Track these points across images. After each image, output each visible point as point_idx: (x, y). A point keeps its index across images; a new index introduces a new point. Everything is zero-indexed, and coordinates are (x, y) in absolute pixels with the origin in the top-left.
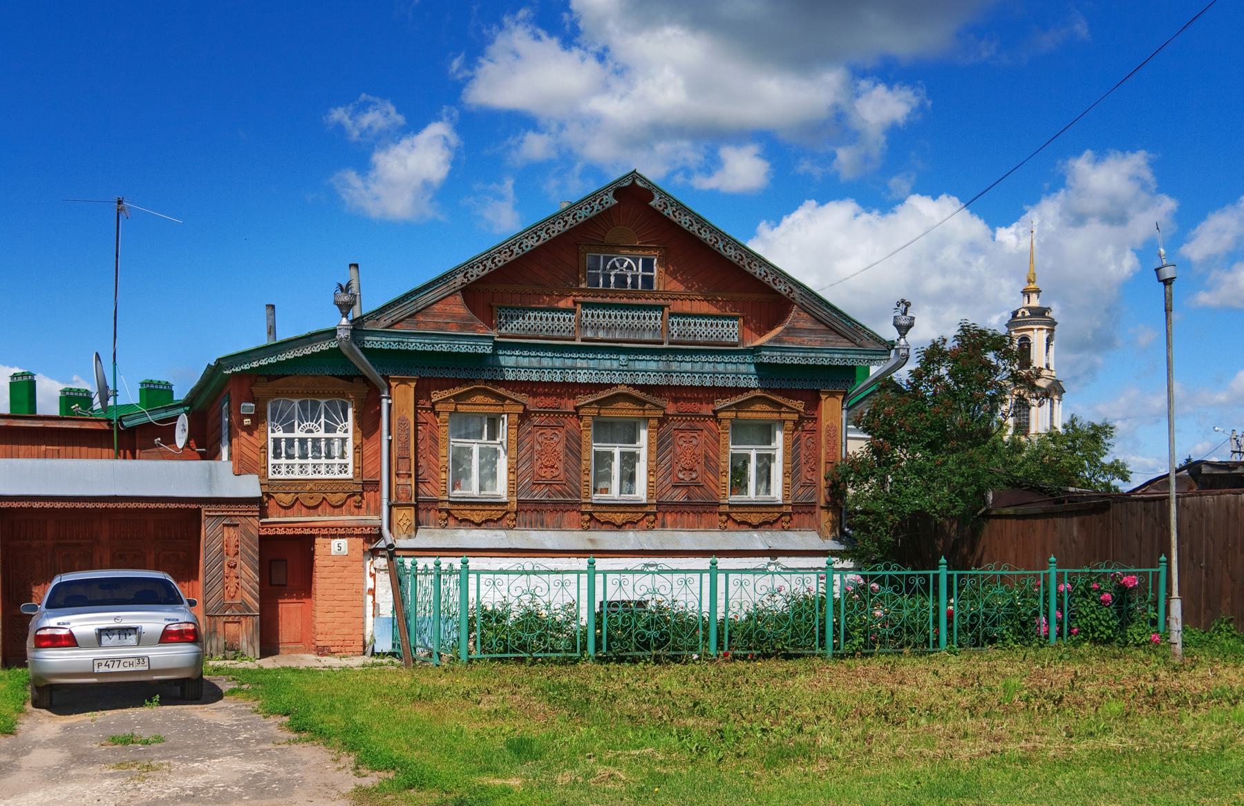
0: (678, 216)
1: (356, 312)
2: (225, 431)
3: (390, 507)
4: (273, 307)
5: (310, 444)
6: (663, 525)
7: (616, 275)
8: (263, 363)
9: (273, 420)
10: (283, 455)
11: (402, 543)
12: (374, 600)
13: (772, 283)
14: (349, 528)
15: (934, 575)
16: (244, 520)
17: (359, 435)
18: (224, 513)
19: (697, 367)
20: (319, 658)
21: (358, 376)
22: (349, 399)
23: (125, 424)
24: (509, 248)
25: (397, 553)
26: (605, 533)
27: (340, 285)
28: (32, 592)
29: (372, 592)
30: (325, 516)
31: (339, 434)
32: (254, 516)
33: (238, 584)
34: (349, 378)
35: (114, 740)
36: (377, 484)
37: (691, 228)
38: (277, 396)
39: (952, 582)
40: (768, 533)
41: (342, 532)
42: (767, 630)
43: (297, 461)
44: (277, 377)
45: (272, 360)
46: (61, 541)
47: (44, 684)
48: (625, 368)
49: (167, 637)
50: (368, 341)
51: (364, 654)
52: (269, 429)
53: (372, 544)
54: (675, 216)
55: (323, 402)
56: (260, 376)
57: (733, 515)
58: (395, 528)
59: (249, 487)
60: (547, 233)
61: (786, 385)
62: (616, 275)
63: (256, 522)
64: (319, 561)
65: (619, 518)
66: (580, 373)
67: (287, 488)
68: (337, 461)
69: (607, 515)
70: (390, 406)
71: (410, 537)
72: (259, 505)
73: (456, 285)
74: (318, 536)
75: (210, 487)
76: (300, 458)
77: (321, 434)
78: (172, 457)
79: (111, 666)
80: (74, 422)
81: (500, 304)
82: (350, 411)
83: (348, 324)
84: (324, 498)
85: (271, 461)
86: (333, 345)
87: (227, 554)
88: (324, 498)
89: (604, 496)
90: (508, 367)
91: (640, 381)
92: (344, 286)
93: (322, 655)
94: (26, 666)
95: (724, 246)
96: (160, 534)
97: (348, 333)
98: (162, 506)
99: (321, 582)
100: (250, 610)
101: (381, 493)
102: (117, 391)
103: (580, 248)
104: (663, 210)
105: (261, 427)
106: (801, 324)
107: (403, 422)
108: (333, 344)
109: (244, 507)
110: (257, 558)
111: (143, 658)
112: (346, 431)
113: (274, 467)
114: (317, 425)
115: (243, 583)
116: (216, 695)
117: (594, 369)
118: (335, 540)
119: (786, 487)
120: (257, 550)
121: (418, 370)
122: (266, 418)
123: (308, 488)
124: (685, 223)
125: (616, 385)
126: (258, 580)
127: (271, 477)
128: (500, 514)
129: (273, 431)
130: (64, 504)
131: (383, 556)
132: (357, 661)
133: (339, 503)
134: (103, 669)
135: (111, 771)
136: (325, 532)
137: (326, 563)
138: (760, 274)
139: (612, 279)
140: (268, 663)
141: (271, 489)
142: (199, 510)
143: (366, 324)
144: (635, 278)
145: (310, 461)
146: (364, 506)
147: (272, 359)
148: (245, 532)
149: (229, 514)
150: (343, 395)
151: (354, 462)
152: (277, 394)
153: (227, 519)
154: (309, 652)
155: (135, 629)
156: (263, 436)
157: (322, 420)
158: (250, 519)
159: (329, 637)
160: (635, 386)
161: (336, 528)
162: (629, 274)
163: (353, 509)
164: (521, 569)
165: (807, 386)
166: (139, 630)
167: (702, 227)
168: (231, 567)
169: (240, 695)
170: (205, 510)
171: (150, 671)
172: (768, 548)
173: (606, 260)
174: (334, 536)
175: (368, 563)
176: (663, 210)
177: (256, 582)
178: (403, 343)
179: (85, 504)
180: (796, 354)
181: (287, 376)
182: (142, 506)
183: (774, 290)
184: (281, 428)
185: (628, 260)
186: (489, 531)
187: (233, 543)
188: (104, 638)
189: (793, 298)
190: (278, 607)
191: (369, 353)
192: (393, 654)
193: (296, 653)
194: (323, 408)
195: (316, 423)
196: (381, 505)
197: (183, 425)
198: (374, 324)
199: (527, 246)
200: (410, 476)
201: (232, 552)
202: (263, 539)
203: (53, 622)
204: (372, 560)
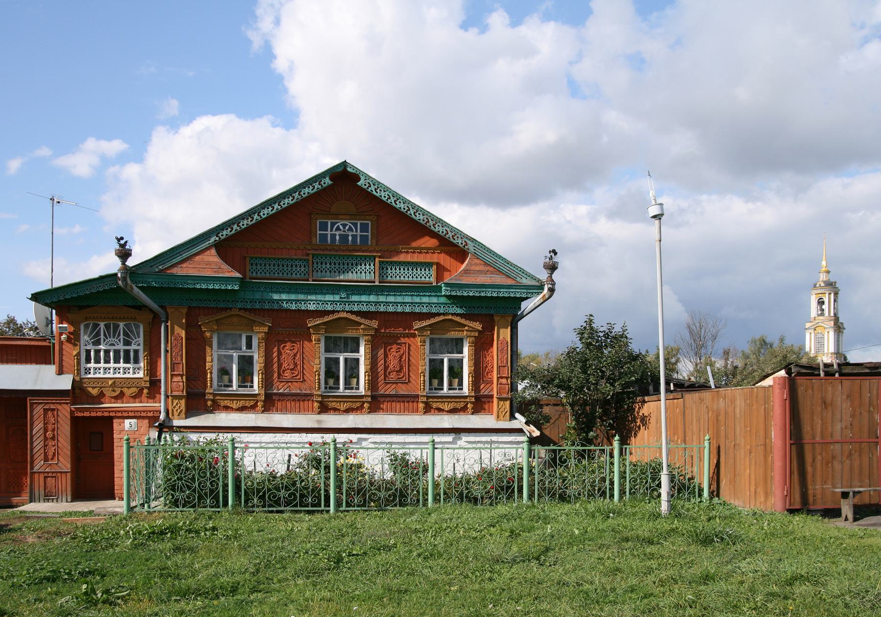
7: (339, 235)
13: (432, 227)
15: (109, 362)
31: (133, 347)
32: (67, 403)
39: (227, 491)
41: (131, 414)
42: (705, 519)
54: (377, 192)
60: (319, 184)
62: (339, 235)
69: (333, 404)
77: (121, 347)
89: (357, 391)
91: (356, 308)
95: (414, 213)
104: (368, 188)
106: (474, 268)
112: (139, 345)
124: (385, 197)
125: (338, 312)
138: (404, 209)
139: (338, 238)
150: (134, 319)
160: (352, 312)
161: (128, 412)
165: (484, 312)
167: (398, 199)
173: (333, 225)
180: (518, 290)
183: (453, 243)
185: (350, 224)
189: (468, 249)
195: (117, 339)
199: (264, 214)
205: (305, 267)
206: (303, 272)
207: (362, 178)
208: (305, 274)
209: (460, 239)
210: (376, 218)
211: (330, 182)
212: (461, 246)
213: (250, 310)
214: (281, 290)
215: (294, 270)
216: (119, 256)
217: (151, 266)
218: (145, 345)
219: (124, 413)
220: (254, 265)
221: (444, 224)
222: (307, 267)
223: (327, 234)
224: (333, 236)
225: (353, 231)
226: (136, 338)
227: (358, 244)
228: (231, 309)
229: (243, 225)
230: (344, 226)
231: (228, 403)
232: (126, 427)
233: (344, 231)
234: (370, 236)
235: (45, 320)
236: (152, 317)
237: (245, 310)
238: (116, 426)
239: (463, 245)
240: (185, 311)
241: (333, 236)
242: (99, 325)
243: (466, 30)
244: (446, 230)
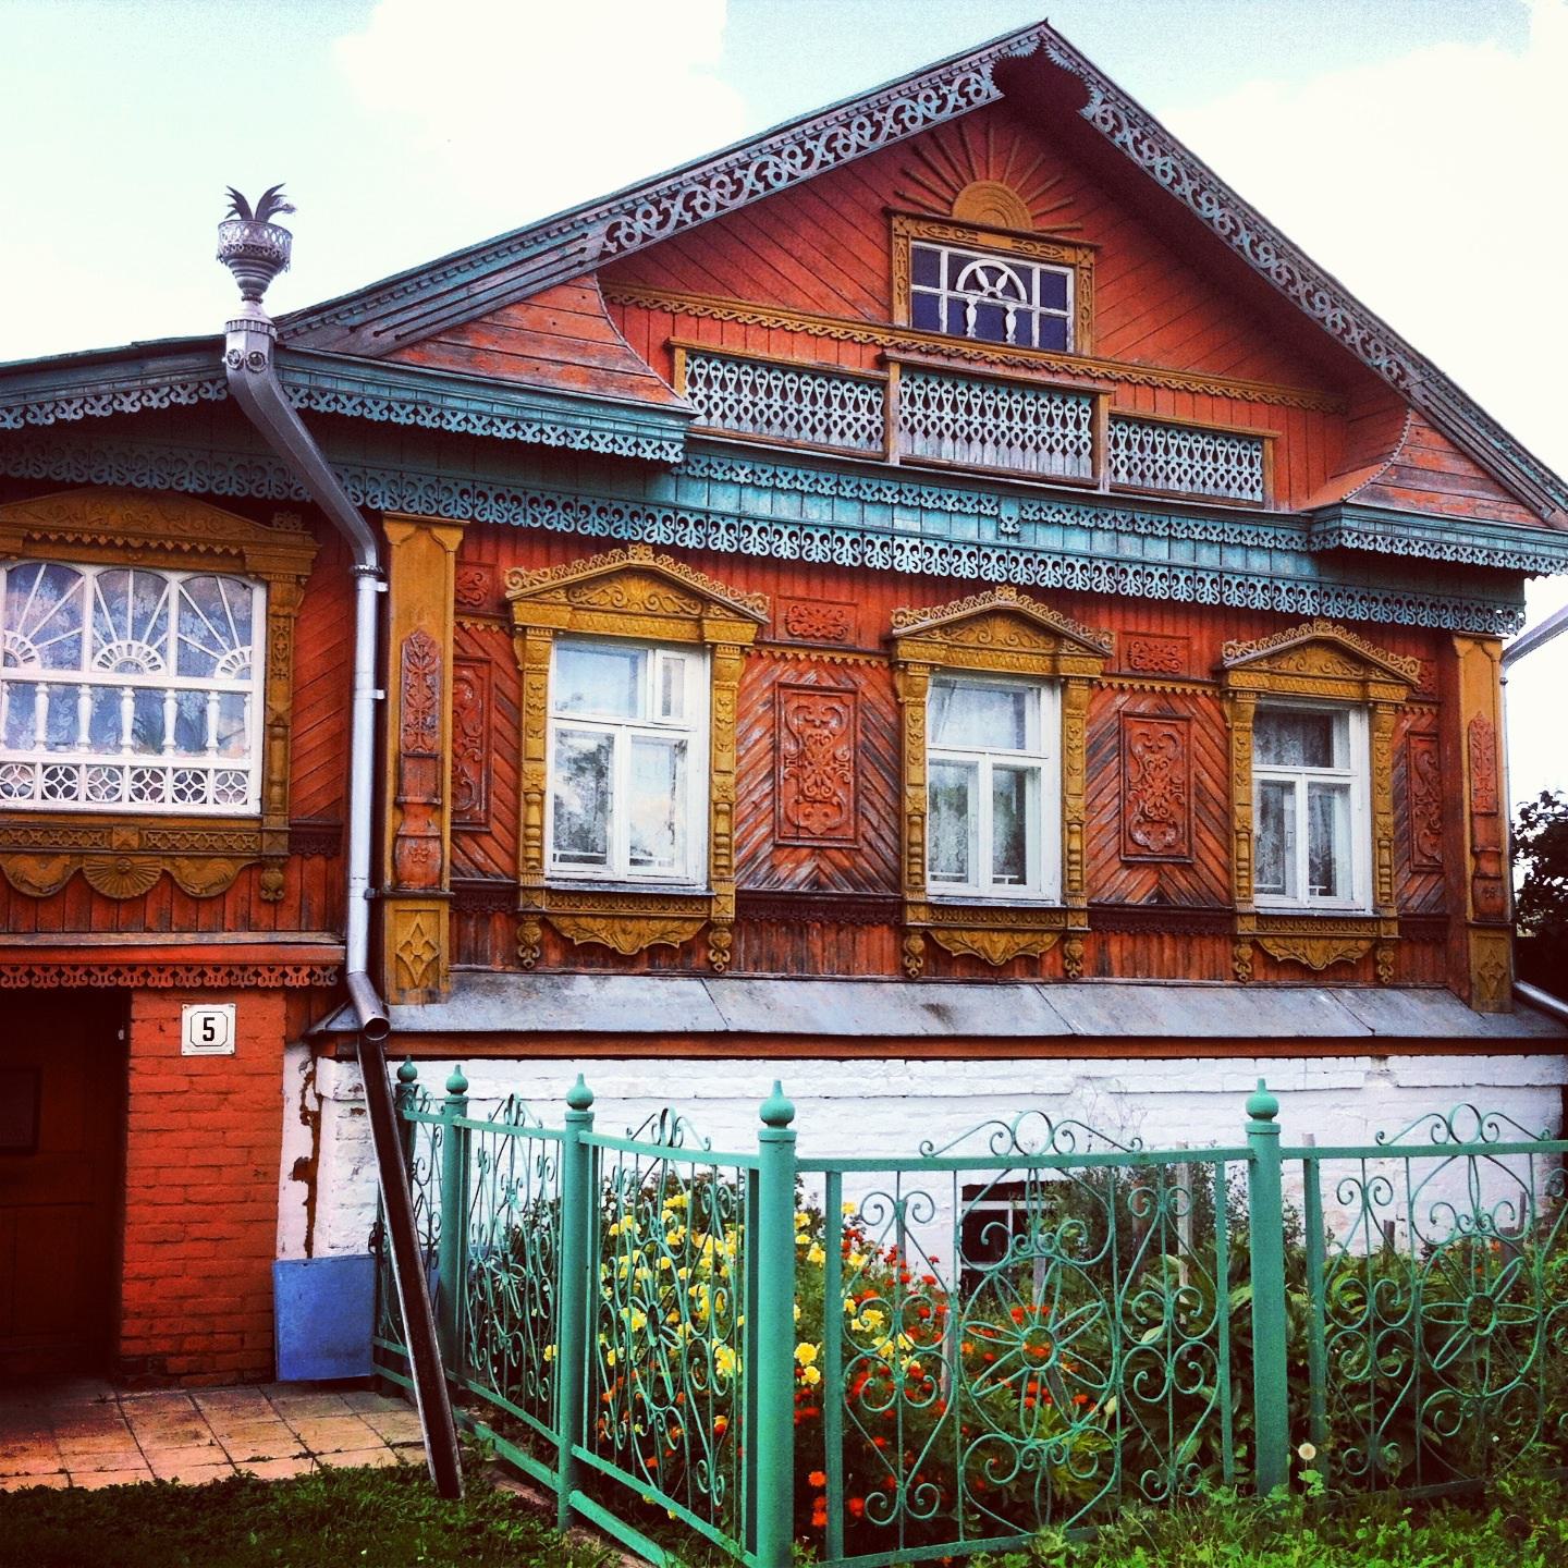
0: (1146, 153)
6: (1103, 970)
11: (411, 1016)
15: (70, 743)
19: (1182, 554)
24: (730, 173)
26: (962, 989)
27: (238, 197)
29: (306, 1170)
31: (221, 681)
34: (257, 510)
37: (1178, 189)
40: (1347, 993)
41: (214, 979)
48: (1013, 542)
54: (1140, 153)
57: (1267, 944)
61: (1380, 614)
62: (979, 306)
65: (998, 947)
66: (900, 546)
69: (966, 937)
70: (382, 600)
73: (586, 256)
81: (695, 343)
90: (717, 514)
92: (253, 206)
95: (1252, 243)
103: (895, 223)
112: (246, 673)
114: (152, 650)
117: (937, 538)
119: (1380, 874)
121: (467, 501)
128: (690, 931)
137: (160, 1082)
139: (972, 315)
144: (1024, 317)
160: (1034, 591)
162: (1011, 306)
164: (1003, 1146)
165: (1427, 620)
172: (1370, 1033)
173: (957, 264)
176: (1112, 133)
185: (1008, 271)
186: (657, 982)
189: (1408, 393)
199: (778, 176)
205: (871, 409)
206: (863, 428)
207: (1097, 97)
208: (870, 438)
209: (1383, 354)
210: (1091, 257)
211: (996, 94)
212: (1388, 378)
213: (702, 558)
214: (806, 488)
215: (835, 417)
217: (353, 329)
218: (271, 675)
219: (154, 974)
220: (701, 383)
221: (1341, 297)
222: (878, 411)
223: (937, 298)
224: (958, 307)
225: (1018, 296)
228: (623, 545)
229: (846, 147)
230: (994, 273)
231: (603, 933)
233: (992, 295)
234: (1070, 321)
237: (680, 553)
238: (141, 1036)
239: (1395, 375)
240: (453, 539)
241: (958, 307)
244: (1344, 319)
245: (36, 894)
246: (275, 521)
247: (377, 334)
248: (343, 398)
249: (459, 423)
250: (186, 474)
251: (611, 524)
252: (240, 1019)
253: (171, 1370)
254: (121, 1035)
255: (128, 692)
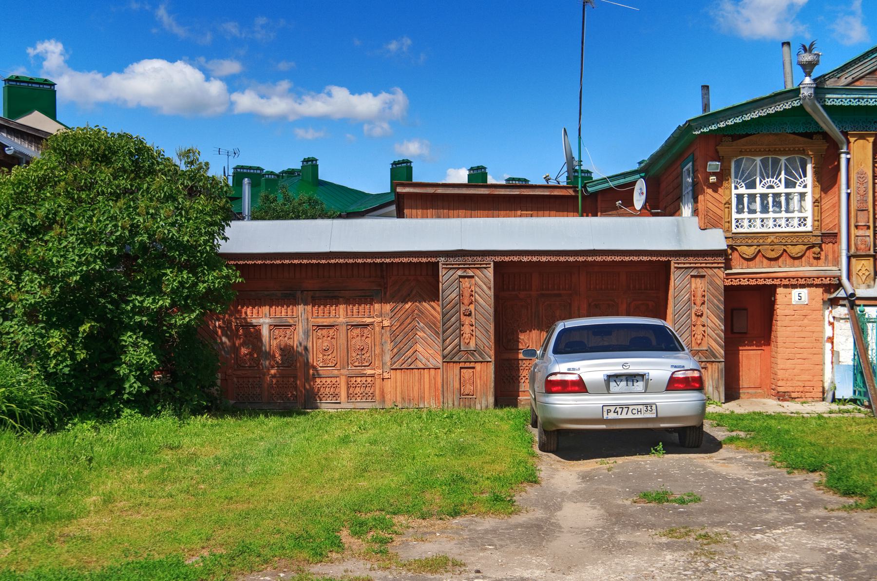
1: (817, 72)
2: (687, 191)
3: (849, 258)
4: (708, 87)
5: (770, 199)
8: (730, 123)
9: (736, 177)
10: (746, 210)
11: (861, 292)
12: (833, 348)
14: (809, 278)
15: (768, 212)
16: (710, 272)
17: (818, 189)
18: (692, 265)
20: (780, 403)
21: (818, 133)
22: (808, 155)
23: (589, 189)
25: (857, 302)
28: (518, 338)
29: (831, 340)
30: (786, 267)
31: (799, 189)
33: (704, 331)
34: (809, 135)
35: (646, 496)
36: (834, 237)
38: (741, 155)
41: (802, 282)
43: (759, 215)
44: (741, 137)
45: (738, 120)
46: (543, 292)
47: (554, 429)
49: (674, 384)
50: (829, 99)
51: (823, 400)
52: (733, 185)
53: (831, 293)
55: (783, 159)
56: (725, 136)
58: (854, 278)
59: (715, 240)
63: (721, 274)
64: (780, 309)
67: (750, 241)
68: (796, 214)
70: (848, 160)
71: (869, 286)
72: (724, 256)
74: (780, 286)
75: (679, 241)
76: (761, 212)
77: (781, 189)
78: (631, 215)
79: (619, 413)
80: (545, 190)
82: (809, 167)
83: (812, 82)
84: (785, 250)
85: (735, 216)
86: (796, 104)
87: (695, 304)
88: (785, 250)
92: (807, 47)
93: (783, 400)
94: (515, 405)
96: (631, 286)
97: (812, 91)
98: (636, 259)
99: (783, 329)
100: (715, 357)
101: (840, 244)
102: (581, 161)
105: (725, 184)
107: (862, 175)
108: (779, 107)
109: (710, 259)
110: (722, 307)
111: (651, 405)
112: (805, 186)
113: (737, 222)
114: (777, 181)
115: (709, 331)
116: (714, 445)
118: (796, 290)
120: (723, 299)
122: (730, 175)
123: (769, 241)
126: (723, 328)
127: (734, 231)
129: (736, 188)
130: (549, 258)
131: (844, 305)
132: (822, 407)
133: (799, 255)
134: (612, 416)
135: (664, 540)
136: (786, 282)
137: (787, 312)
140: (734, 407)
141: (735, 241)
142: (669, 262)
143: (827, 82)
145: (771, 215)
146: (823, 257)
147: (738, 119)
148: (711, 283)
149: (697, 265)
150: (803, 152)
151: (813, 215)
152: (741, 153)
153: (695, 271)
154: (769, 396)
155: (642, 376)
156: (727, 192)
157: (783, 176)
158: (716, 270)
159: (789, 383)
161: (797, 278)
163: (812, 260)
166: (646, 377)
168: (698, 316)
169: (739, 443)
170: (673, 260)
171: (658, 419)
174: (794, 286)
175: (827, 312)
177: (722, 330)
178: (863, 99)
179: (567, 258)
181: (751, 135)
182: (618, 259)
184: (743, 185)
187: (699, 293)
188: (613, 384)
190: (739, 354)
191: (831, 110)
192: (854, 401)
193: (756, 398)
194: (783, 168)
195: (776, 179)
196: (839, 256)
197: (641, 189)
198: (835, 82)
200: (868, 227)
201: (699, 302)
202: (729, 291)
203: (563, 367)
204: (830, 308)
216: (107, 76)
226: (801, 178)
227: (694, 133)
232: (793, 300)
235: (799, 66)
236: (826, 147)
242: (780, 160)
243: (306, 161)
245: (747, 257)
246: (814, 138)
247: (846, 78)
248: (844, 100)
249: (873, 103)
250: (787, 127)
251: (795, 127)
252: (809, 293)
253: (793, 397)
254: (773, 299)
255: (746, 195)
